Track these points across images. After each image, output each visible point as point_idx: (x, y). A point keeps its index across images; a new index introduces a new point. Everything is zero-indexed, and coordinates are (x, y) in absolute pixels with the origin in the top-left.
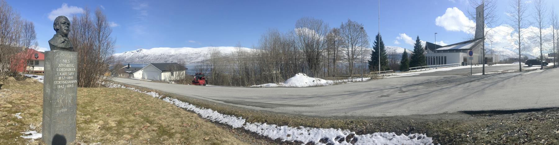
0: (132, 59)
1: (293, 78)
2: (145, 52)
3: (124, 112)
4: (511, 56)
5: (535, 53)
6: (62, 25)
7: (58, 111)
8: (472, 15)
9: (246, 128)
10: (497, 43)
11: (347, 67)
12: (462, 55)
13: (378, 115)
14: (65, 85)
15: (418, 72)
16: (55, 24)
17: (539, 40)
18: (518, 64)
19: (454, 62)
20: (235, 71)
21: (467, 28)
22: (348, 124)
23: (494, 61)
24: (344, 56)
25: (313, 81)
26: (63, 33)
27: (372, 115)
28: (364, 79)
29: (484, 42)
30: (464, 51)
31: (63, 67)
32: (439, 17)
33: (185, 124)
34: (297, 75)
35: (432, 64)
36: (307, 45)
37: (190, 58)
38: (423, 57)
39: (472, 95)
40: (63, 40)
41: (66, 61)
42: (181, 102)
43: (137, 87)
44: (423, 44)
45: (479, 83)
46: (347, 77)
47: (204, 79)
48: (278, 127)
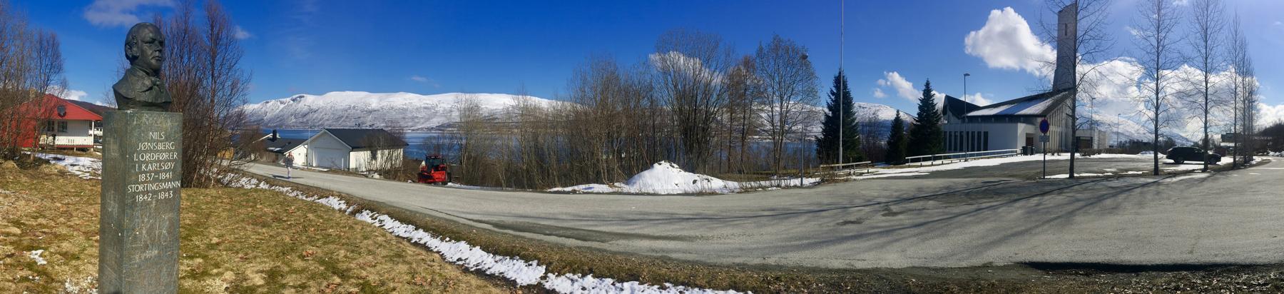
0: (280, 119)
1: (646, 173)
2: (310, 101)
3: (279, 249)
4: (1136, 137)
5: (1191, 131)
6: (146, 46)
7: (137, 257)
8: (1049, 33)
9: (547, 286)
10: (1104, 103)
11: (768, 149)
12: (1022, 129)
13: (837, 264)
14: (155, 192)
15: (927, 167)
16: (129, 44)
17: (1201, 100)
18: (1150, 155)
19: (1005, 146)
20: (513, 153)
21: (1037, 64)
22: (769, 283)
23: (1095, 147)
24: (762, 125)
25: (695, 182)
26: (149, 65)
27: (823, 263)
28: (807, 181)
29: (1074, 100)
30: (1028, 119)
31: (151, 151)
32: (973, 33)
33: (418, 280)
34: (656, 165)
35: (955, 151)
36: (681, 96)
37: (413, 118)
38: (938, 132)
39: (1046, 227)
40: (148, 83)
41: (155, 136)
42: (397, 223)
43: (296, 187)
44: (939, 99)
45: (1060, 197)
46: (767, 177)
47: (443, 169)
48: (618, 285)
